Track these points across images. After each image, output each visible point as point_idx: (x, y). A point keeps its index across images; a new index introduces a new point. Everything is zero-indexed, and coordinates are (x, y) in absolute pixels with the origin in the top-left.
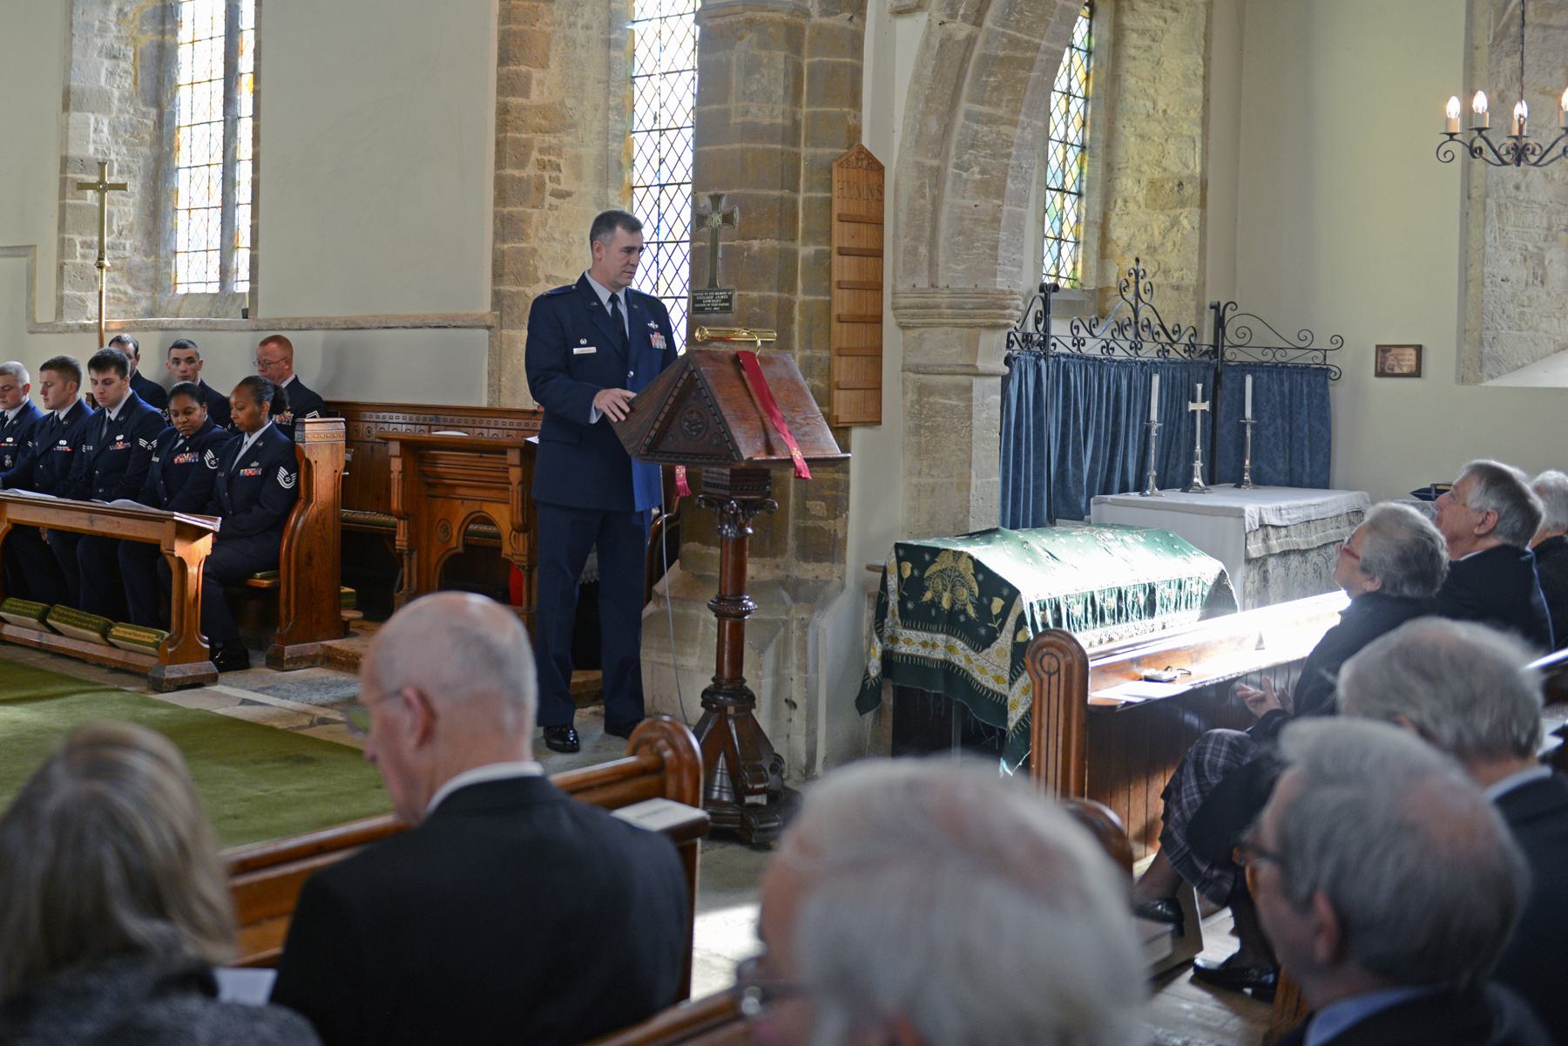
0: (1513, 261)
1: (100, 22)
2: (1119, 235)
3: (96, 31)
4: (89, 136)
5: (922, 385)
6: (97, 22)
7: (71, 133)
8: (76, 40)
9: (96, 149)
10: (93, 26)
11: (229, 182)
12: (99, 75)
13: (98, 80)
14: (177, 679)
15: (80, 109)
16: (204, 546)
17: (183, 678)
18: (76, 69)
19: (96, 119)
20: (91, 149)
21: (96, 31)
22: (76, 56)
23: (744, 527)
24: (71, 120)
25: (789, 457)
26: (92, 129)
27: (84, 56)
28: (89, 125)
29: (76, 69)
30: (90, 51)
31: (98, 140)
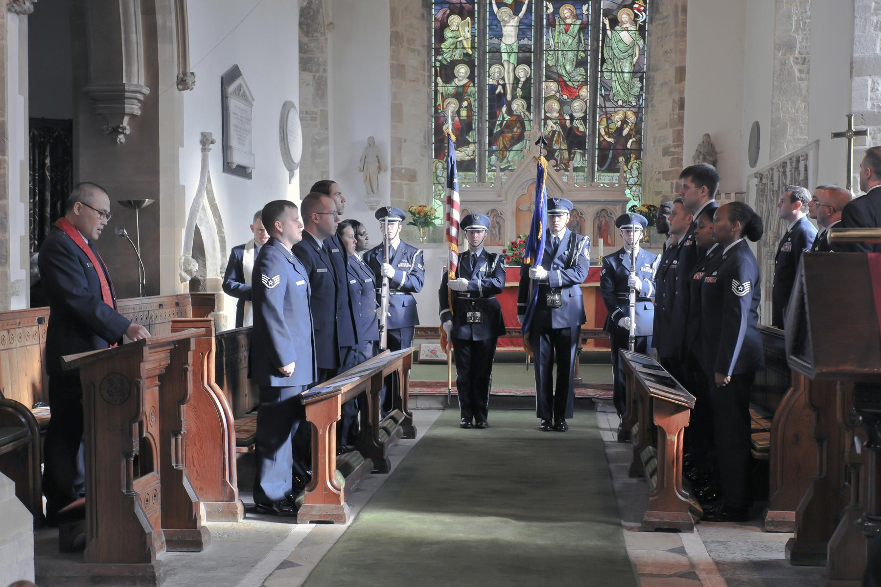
0: (16, 289)
1: (876, 3)
2: (364, 230)
3: (872, 11)
4: (867, 94)
5: (875, 244)
6: (873, 4)
7: (854, 94)
8: (857, 21)
9: (873, 105)
10: (870, 7)
11: (549, 180)
12: (875, 45)
13: (874, 50)
14: (654, 523)
15: (861, 74)
16: (683, 419)
17: (659, 523)
18: (858, 44)
19: (873, 81)
20: (869, 105)
21: (872, 11)
22: (858, 33)
23: (49, 427)
24: (853, 83)
25: (157, 377)
26: (869, 89)
27: (864, 32)
28: (867, 86)
29: (858, 44)
30: (867, 28)
31: (874, 98)
